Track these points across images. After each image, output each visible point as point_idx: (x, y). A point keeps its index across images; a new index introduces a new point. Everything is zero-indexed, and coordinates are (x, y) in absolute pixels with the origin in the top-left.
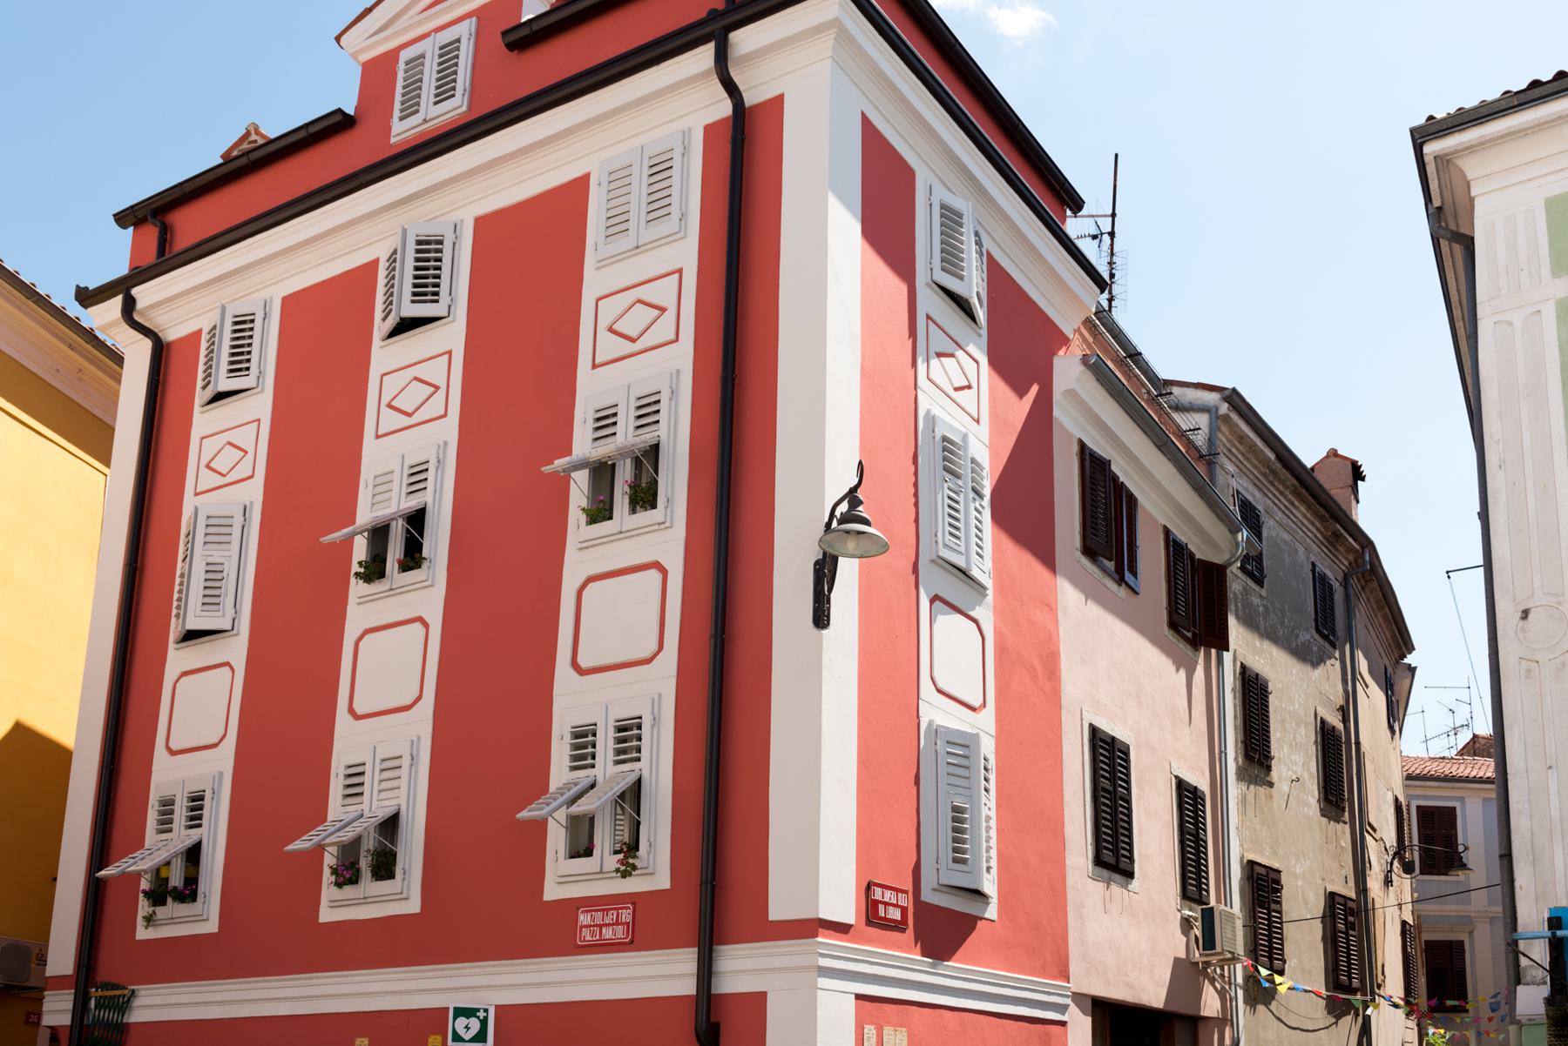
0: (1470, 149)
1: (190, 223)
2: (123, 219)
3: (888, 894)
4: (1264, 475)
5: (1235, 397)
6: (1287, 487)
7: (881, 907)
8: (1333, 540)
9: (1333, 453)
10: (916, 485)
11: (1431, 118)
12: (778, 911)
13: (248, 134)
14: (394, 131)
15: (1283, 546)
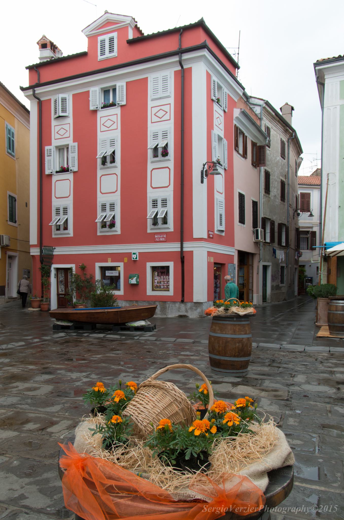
0: (325, 68)
2: (27, 68)
4: (272, 118)
6: (276, 120)
8: (286, 131)
9: (287, 104)
10: (111, 13)
11: (318, 61)
12: (195, 236)
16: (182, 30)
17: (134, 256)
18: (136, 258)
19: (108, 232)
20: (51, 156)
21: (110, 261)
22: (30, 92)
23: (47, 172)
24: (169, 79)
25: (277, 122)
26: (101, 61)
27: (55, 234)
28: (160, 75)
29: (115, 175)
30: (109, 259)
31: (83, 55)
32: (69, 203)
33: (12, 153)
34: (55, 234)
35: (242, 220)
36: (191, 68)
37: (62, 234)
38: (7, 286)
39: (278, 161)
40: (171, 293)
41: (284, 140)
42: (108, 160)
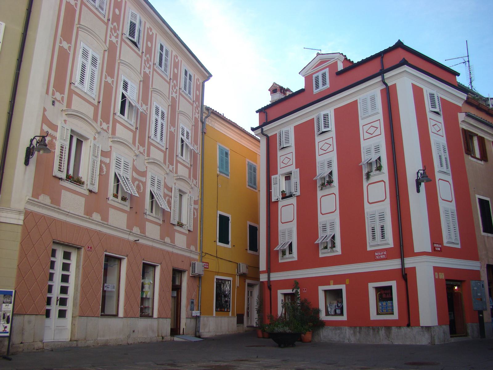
1: (273, 113)
2: (257, 112)
3: (437, 245)
7: (436, 248)
13: (273, 84)
14: (314, 92)
21: (332, 283)
22: (259, 131)
23: (273, 200)
27: (371, 246)
28: (367, 95)
31: (302, 91)
36: (395, 84)
38: (246, 315)
40: (395, 316)
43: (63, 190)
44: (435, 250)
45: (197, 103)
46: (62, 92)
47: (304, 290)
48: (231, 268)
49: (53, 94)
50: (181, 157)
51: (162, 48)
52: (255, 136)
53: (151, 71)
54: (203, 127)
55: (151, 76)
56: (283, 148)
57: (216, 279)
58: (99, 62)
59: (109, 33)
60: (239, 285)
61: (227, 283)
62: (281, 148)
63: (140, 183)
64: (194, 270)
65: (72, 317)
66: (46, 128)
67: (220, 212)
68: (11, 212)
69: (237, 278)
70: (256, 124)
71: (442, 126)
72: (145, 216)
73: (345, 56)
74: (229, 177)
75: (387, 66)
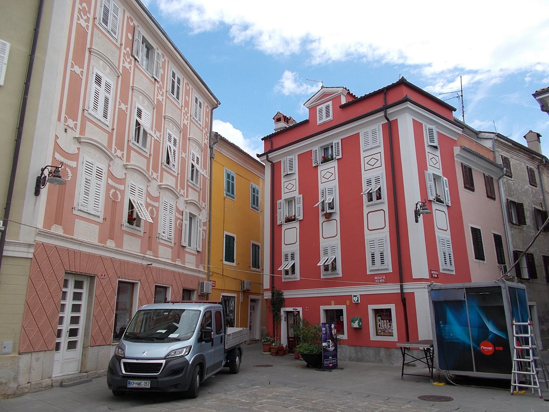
1: (278, 142)
2: (262, 139)
3: (434, 272)
4: (509, 149)
5: (499, 135)
10: (327, 87)
11: (536, 91)
13: (278, 113)
15: (517, 165)
16: (385, 90)
17: (355, 299)
18: (358, 301)
19: (330, 274)
20: (281, 208)
21: (334, 303)
22: (265, 157)
23: (279, 223)
24: (377, 131)
25: (518, 151)
26: (320, 125)
28: (369, 129)
29: (335, 220)
30: (332, 301)
31: (306, 122)
32: (296, 248)
33: (257, 207)
34: (285, 278)
35: (480, 255)
37: (291, 278)
39: (527, 189)
41: (532, 167)
42: (374, 197)
43: (76, 220)
44: (432, 277)
45: (206, 129)
46: (75, 119)
47: (306, 309)
48: (235, 286)
49: (66, 121)
50: (191, 181)
51: (174, 75)
52: (260, 162)
53: (164, 98)
54: (212, 153)
55: (164, 103)
56: (287, 174)
57: (222, 296)
58: (113, 87)
59: (122, 58)
60: (243, 300)
61: (232, 299)
62: (285, 174)
63: (153, 208)
64: (202, 289)
65: (83, 347)
66: (58, 156)
67: (226, 233)
68: (20, 245)
69: (241, 295)
70: (261, 151)
71: (439, 159)
72: (158, 240)
73: (348, 90)
74: (235, 200)
75: (390, 102)
